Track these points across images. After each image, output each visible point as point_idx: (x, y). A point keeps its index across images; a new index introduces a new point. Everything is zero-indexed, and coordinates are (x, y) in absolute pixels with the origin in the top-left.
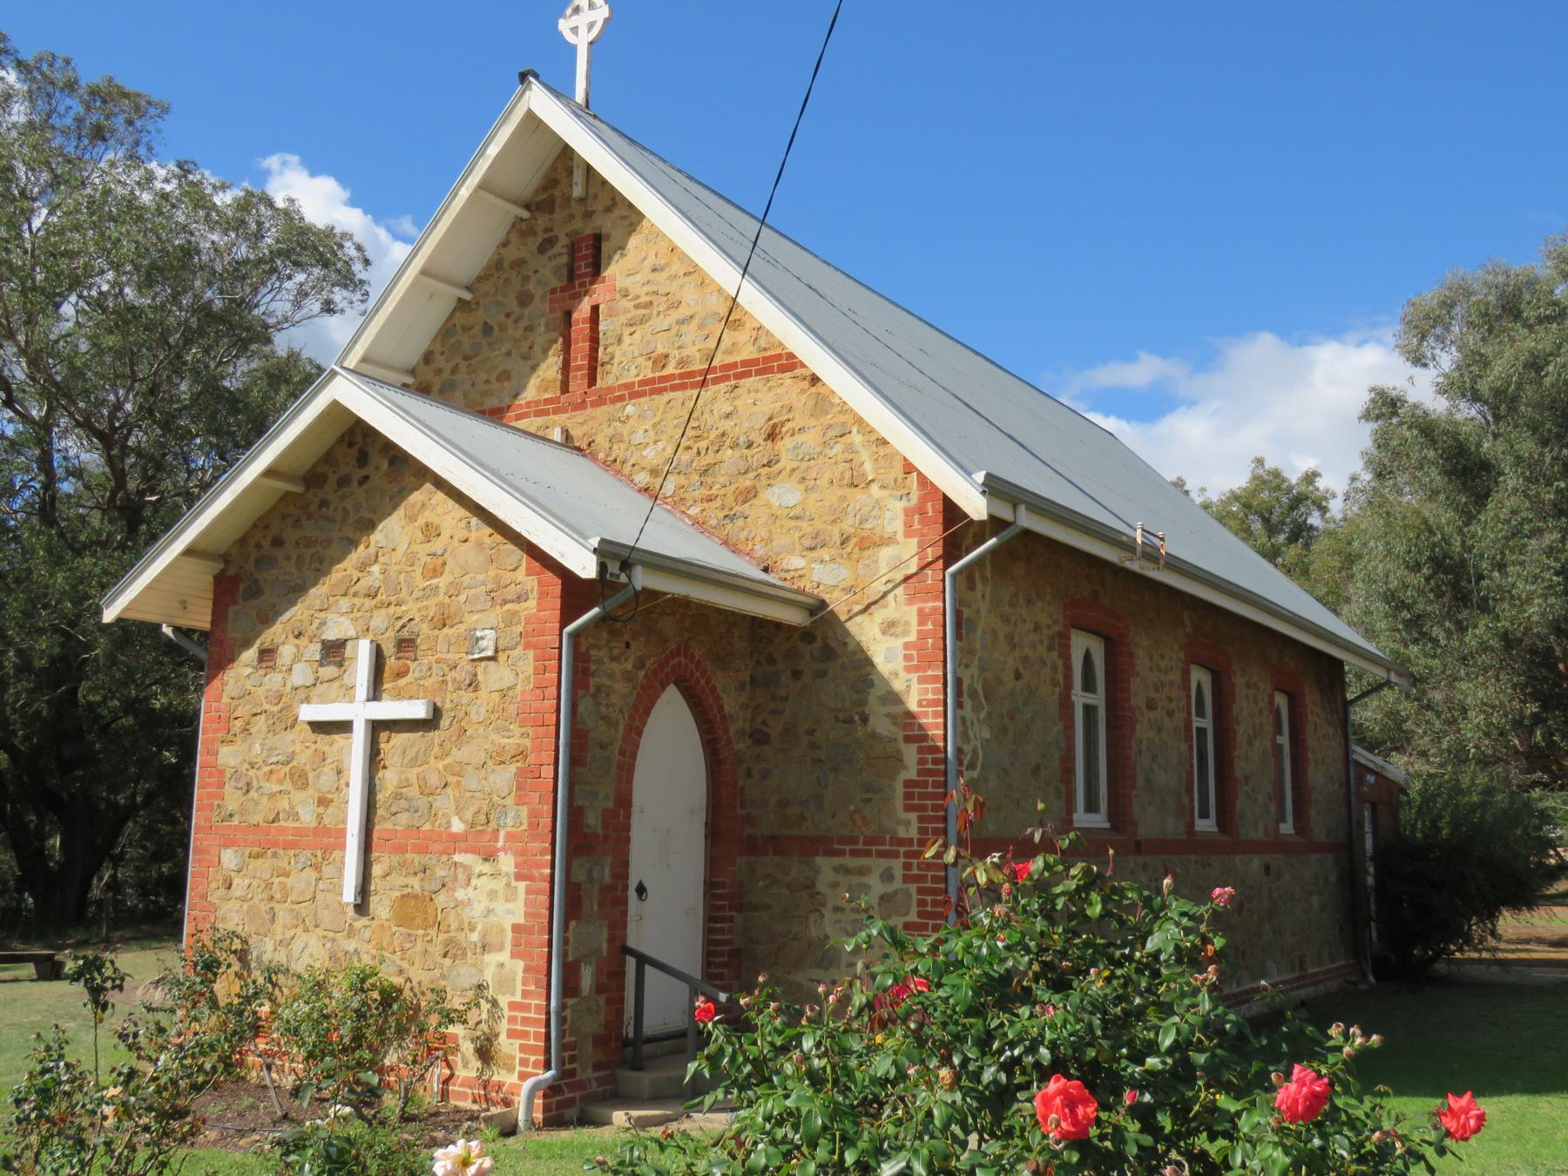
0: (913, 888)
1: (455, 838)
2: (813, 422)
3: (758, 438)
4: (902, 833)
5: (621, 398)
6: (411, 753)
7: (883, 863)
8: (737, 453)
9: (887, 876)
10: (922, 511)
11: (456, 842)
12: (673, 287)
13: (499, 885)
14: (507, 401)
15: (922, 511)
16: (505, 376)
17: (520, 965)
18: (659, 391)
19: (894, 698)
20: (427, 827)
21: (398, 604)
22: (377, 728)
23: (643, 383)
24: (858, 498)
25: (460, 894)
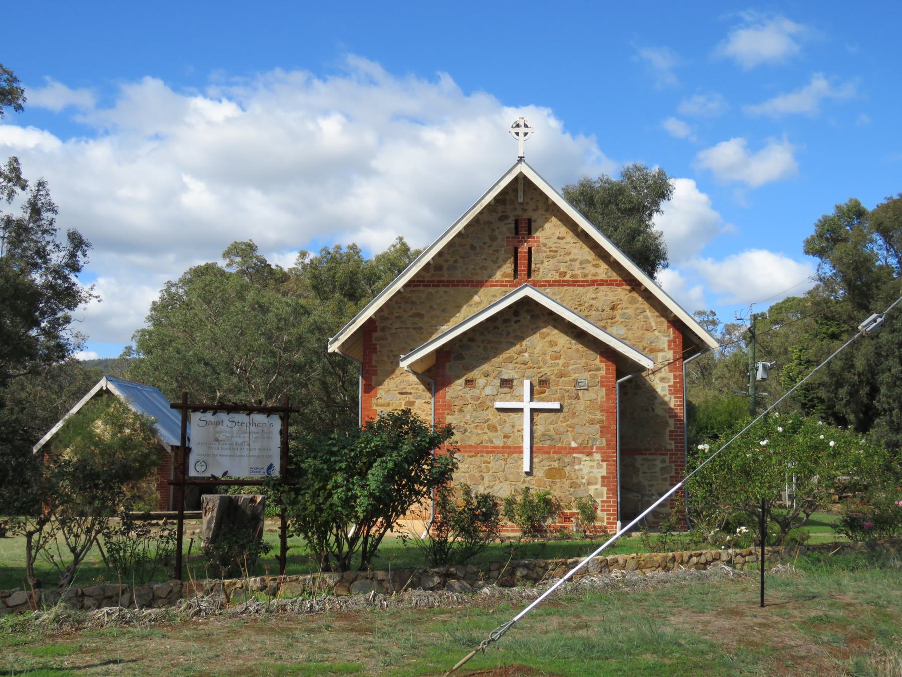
0: (673, 465)
1: (574, 449)
2: (630, 306)
3: (607, 309)
4: (669, 447)
5: (544, 286)
6: (550, 420)
7: (662, 457)
8: (598, 313)
9: (663, 461)
10: (674, 342)
11: (574, 450)
12: (568, 246)
13: (594, 464)
14: (486, 278)
15: (674, 342)
16: (484, 268)
17: (605, 489)
18: (562, 285)
19: (665, 403)
20: (560, 445)
21: (539, 368)
22: (533, 411)
23: (554, 281)
24: (648, 335)
25: (577, 467)
